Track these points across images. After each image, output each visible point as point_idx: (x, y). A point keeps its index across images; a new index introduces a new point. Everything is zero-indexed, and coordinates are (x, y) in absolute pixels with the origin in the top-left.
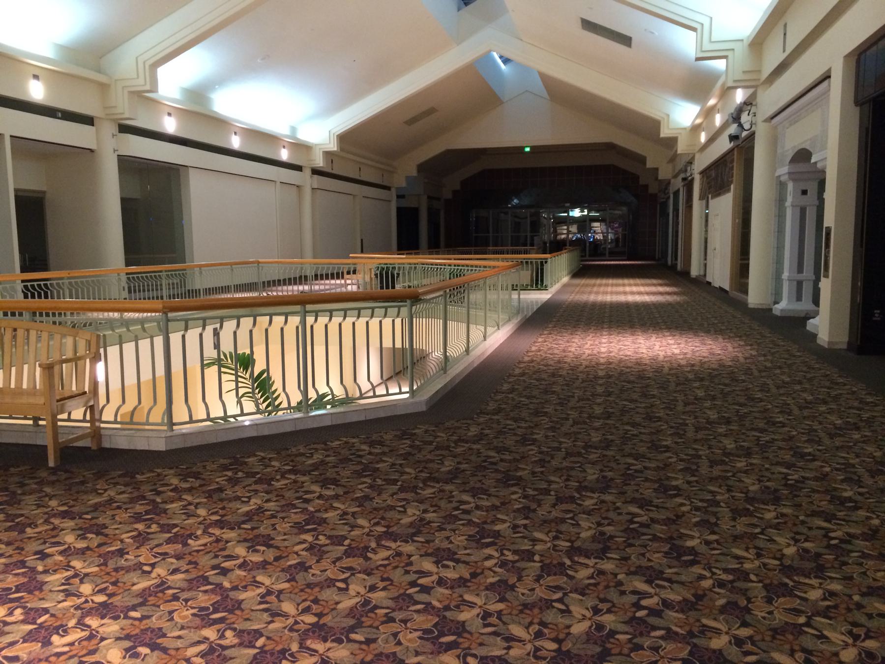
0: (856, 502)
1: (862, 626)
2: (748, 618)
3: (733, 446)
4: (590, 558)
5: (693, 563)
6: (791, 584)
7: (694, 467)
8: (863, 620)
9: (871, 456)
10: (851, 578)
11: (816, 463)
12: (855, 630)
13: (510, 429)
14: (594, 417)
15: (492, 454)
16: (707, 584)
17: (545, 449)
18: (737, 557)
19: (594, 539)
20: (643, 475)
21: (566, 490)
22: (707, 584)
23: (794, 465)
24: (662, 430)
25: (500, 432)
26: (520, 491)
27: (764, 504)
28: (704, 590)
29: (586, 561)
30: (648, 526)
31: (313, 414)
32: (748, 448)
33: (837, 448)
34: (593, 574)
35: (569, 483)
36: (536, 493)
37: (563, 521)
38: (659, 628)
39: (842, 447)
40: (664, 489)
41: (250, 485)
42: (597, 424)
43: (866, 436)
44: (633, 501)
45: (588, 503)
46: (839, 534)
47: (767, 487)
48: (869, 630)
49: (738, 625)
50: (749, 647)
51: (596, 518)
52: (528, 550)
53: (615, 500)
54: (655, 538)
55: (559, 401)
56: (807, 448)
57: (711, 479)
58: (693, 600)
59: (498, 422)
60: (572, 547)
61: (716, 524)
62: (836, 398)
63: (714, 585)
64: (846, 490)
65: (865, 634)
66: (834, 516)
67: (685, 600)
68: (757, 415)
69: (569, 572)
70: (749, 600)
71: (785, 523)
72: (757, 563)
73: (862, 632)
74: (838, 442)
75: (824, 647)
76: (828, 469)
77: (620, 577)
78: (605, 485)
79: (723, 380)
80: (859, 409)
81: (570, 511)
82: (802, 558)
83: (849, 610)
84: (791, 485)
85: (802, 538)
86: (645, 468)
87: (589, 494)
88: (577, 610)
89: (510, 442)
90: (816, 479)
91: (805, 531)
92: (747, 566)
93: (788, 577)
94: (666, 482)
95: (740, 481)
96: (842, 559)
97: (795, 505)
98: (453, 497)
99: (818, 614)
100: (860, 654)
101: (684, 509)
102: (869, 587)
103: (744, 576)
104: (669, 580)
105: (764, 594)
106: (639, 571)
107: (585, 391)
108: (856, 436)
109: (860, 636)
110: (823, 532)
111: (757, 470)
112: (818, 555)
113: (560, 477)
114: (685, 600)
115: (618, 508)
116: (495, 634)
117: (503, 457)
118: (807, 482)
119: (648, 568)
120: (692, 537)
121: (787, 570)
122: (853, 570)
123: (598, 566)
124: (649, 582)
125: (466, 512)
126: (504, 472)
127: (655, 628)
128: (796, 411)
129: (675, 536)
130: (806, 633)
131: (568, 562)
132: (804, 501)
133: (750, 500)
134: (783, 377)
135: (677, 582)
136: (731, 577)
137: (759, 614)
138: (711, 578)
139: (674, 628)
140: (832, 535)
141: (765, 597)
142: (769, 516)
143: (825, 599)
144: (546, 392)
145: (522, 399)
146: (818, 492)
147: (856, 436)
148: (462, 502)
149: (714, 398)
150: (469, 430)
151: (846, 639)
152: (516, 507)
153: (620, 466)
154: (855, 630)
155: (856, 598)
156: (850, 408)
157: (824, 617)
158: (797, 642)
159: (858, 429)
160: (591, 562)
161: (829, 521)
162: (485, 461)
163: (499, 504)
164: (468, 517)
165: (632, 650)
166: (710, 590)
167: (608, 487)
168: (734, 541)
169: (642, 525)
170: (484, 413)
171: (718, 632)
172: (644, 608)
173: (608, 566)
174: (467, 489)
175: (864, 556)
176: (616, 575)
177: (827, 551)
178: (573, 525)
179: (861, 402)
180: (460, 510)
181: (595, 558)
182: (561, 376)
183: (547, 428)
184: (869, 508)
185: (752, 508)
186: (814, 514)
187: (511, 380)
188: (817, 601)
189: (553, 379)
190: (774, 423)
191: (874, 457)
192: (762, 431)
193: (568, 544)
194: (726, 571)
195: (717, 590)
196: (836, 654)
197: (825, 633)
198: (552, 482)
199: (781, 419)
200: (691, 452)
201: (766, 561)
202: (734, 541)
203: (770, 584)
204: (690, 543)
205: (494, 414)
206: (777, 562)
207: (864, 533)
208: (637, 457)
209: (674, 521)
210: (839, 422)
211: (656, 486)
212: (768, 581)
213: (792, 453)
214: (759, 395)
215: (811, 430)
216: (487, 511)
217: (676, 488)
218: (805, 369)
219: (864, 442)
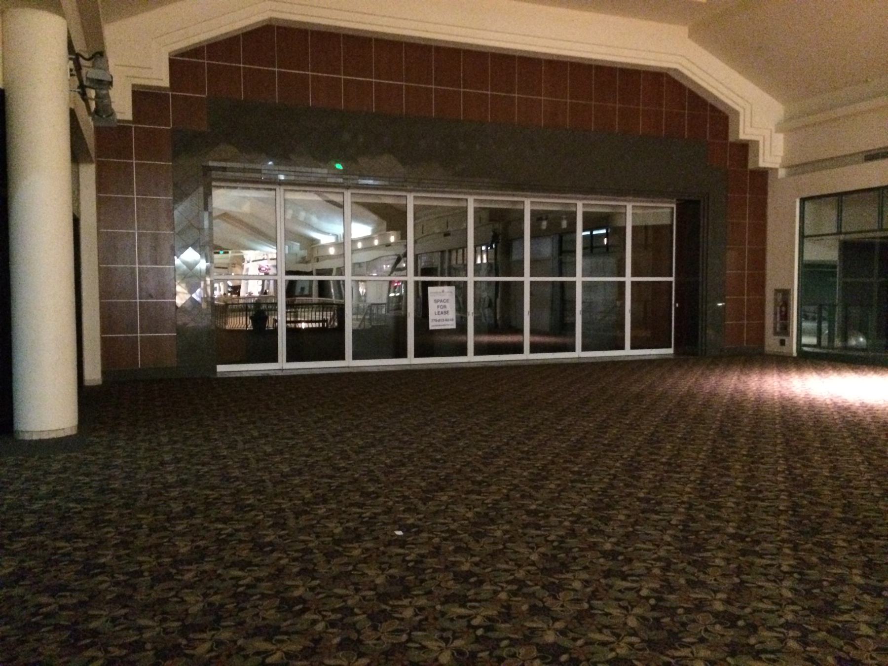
1: (449, 629)
2: (363, 649)
3: (288, 469)
4: (205, 632)
5: (303, 611)
6: (388, 608)
7: (282, 521)
8: (447, 624)
10: (377, 538)
11: (379, 499)
12: (444, 635)
13: (64, 555)
14: (174, 518)
15: (44, 599)
16: (320, 627)
18: (303, 541)
19: (204, 612)
20: (258, 591)
21: (167, 637)
22: (320, 627)
24: (284, 567)
25: (63, 518)
26: (100, 654)
28: (320, 633)
29: (190, 567)
30: (253, 586)
33: (362, 461)
34: (212, 646)
35: (162, 560)
36: (124, 652)
37: (166, 601)
38: (256, 595)
40: (259, 547)
42: (175, 493)
44: (234, 565)
45: (188, 576)
47: (318, 494)
48: (454, 632)
49: (355, 658)
50: (318, 590)
52: (136, 641)
53: (215, 568)
54: (264, 596)
55: (124, 475)
57: (300, 530)
58: (312, 645)
59: (23, 601)
60: (184, 625)
62: (381, 441)
63: (326, 627)
64: (408, 519)
65: (453, 635)
66: (364, 504)
67: (270, 574)
69: (187, 652)
70: (358, 632)
71: (371, 556)
72: (357, 598)
73: (449, 634)
74: (361, 457)
75: (425, 656)
76: (391, 503)
77: (240, 642)
78: (200, 554)
80: (373, 432)
81: (171, 589)
82: (391, 584)
83: (436, 619)
84: (366, 522)
86: (237, 530)
87: (186, 567)
88: (190, 599)
89: (67, 575)
90: (350, 483)
91: (386, 559)
92: (311, 545)
95: (298, 493)
96: (420, 577)
98: (26, 601)
99: (415, 629)
100: (453, 654)
101: (282, 562)
102: (445, 596)
103: (350, 611)
104: (286, 633)
105: (325, 558)
106: (257, 632)
107: (152, 461)
109: (449, 638)
110: (402, 557)
112: (403, 578)
113: (152, 618)
114: (270, 574)
115: (220, 575)
116: (128, 629)
117: (63, 601)
118: (425, 560)
120: (297, 587)
121: (383, 597)
122: (430, 585)
123: (216, 637)
124: (269, 639)
125: (47, 616)
126: (67, 628)
127: (252, 596)
128: (383, 478)
129: (281, 589)
130: (410, 648)
133: (338, 542)
135: (293, 633)
136: (339, 616)
137: (370, 642)
138: (323, 620)
139: (266, 592)
140: (364, 515)
141: (371, 626)
142: (356, 552)
143: (416, 615)
144: (102, 491)
145: (71, 505)
148: (40, 606)
149: (281, 453)
150: (22, 520)
151: (440, 644)
152: (108, 597)
153: (225, 584)
154: (444, 635)
155: (438, 607)
157: (420, 631)
158: (405, 658)
161: (362, 508)
164: (53, 621)
165: (239, 611)
166: (325, 632)
167: (219, 619)
169: (248, 586)
170: (50, 473)
171: (297, 587)
172: (242, 586)
173: (225, 635)
175: (435, 570)
176: (235, 642)
177: (409, 573)
178: (177, 602)
179: (400, 442)
180: (39, 615)
181: (210, 630)
182: (114, 491)
183: (116, 545)
186: (352, 505)
187: (35, 507)
188: (411, 618)
189: (108, 472)
190: (339, 469)
191: (421, 487)
193: (180, 623)
194: (334, 611)
195: (330, 630)
196: (436, 660)
197: (424, 643)
198: (144, 562)
199: (343, 465)
200: (275, 507)
201: (364, 593)
204: (297, 593)
205: (34, 534)
206: (331, 539)
207: (430, 552)
208: (226, 520)
209: (277, 576)
211: (251, 545)
212: (370, 612)
214: (320, 445)
215: (343, 451)
216: (86, 551)
217: (270, 544)
219: (411, 475)
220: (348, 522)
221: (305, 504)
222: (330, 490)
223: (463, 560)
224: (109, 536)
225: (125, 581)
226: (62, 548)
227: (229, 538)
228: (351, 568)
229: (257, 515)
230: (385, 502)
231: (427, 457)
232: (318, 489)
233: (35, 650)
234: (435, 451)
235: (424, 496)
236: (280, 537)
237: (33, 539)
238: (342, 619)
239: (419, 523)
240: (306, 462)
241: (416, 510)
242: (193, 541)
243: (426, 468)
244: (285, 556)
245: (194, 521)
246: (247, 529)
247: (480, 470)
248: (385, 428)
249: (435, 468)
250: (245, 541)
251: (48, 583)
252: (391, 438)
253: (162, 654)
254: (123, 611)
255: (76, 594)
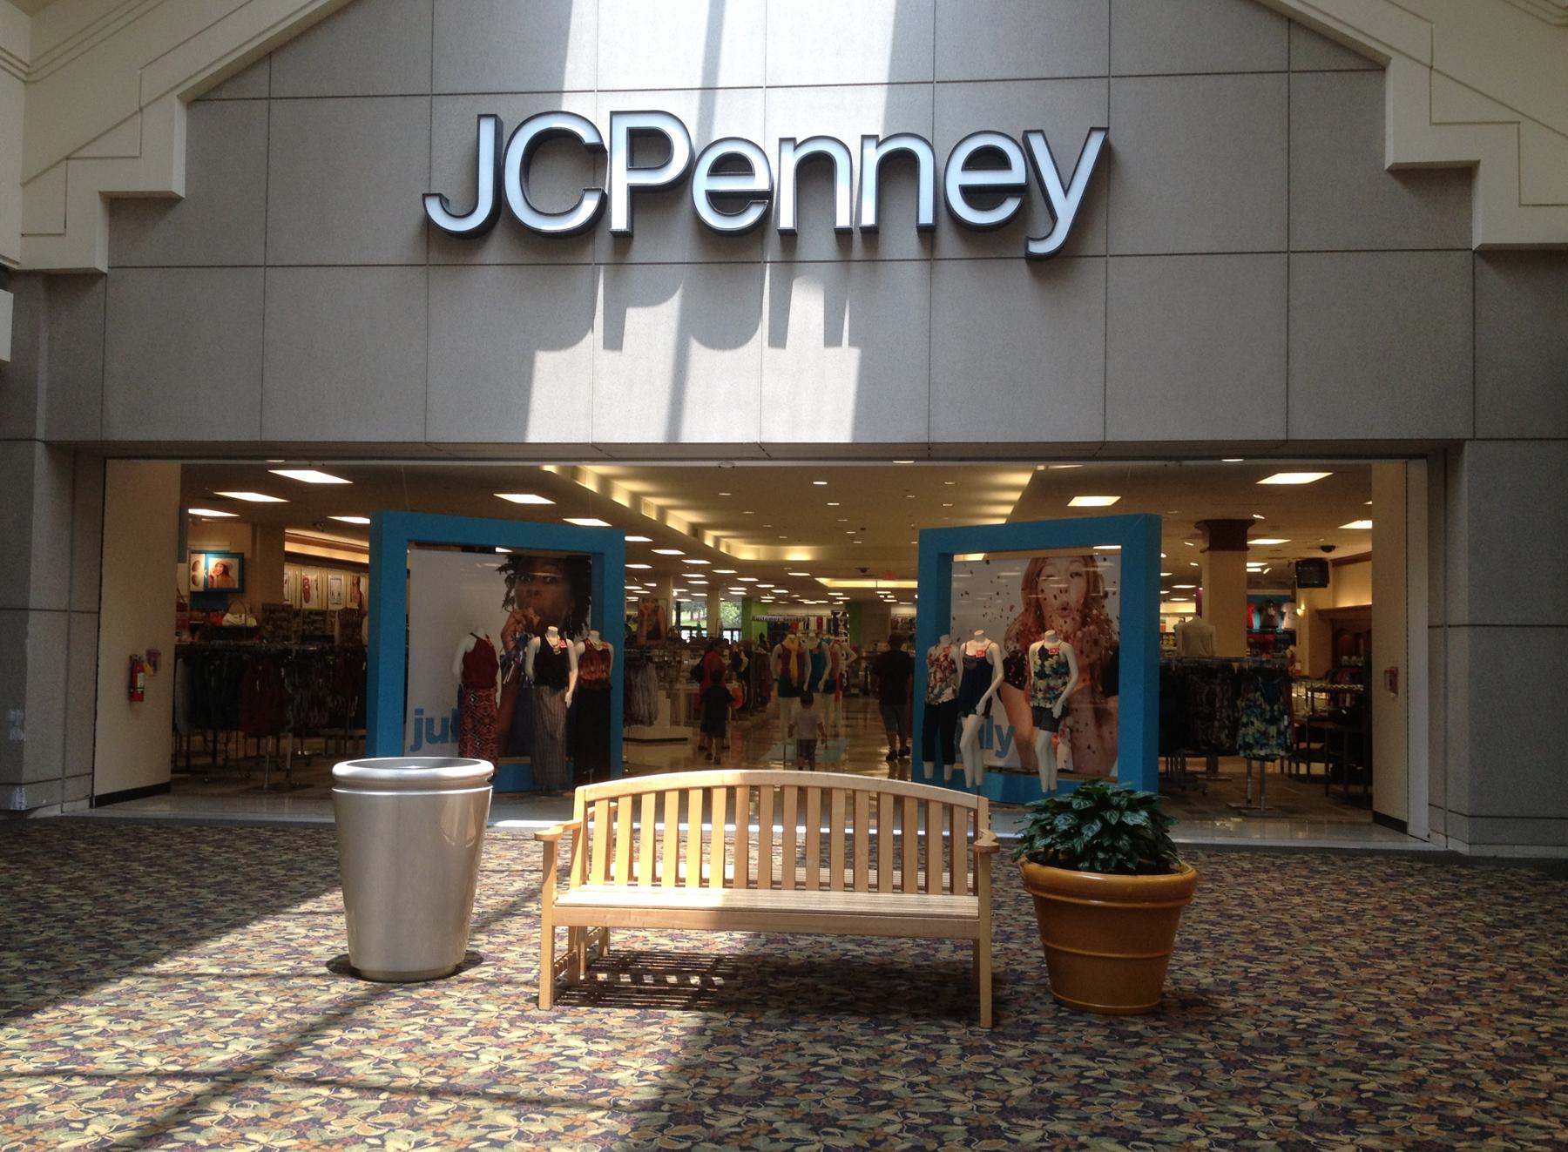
0: (1479, 1124)
6: (1312, 1140)
9: (1486, 1047)
10: (1391, 1133)
11: (1400, 1060)
17: (919, 1121)
23: (1365, 1066)
24: (1154, 1066)
26: (897, 1119)
27: (1332, 1133)
31: (1108, 501)
32: (1234, 983)
39: (1370, 981)
41: (375, 1113)
43: (1472, 1014)
46: (1372, 1086)
51: (1029, 1073)
53: (1076, 1132)
55: (914, 1054)
56: (1379, 1035)
59: (797, 1049)
60: (1004, 1107)
61: (1203, 1079)
64: (1460, 1106)
66: (1304, 1006)
68: (1240, 938)
71: (1298, 1075)
76: (1423, 1071)
79: (1205, 915)
81: (988, 1064)
82: (1264, 1040)
85: (1324, 1092)
87: (1023, 1122)
93: (1308, 1134)
94: (1157, 1100)
97: (1383, 1133)
108: (1457, 1014)
110: (1350, 1084)
111: (1305, 1076)
115: (1057, 1060)
119: (1119, 1129)
120: (894, 1079)
126: (856, 1085)
128: (1346, 972)
131: (1004, 1125)
132: (1268, 993)
134: (1309, 911)
146: (1341, 1037)
147: (1457, 1014)
153: (1064, 1072)
156: (1434, 965)
159: (1392, 956)
160: (1037, 1123)
162: (815, 1064)
163: (876, 1057)
168: (1231, 1097)
174: (797, 1116)
184: (1505, 1135)
185: (1312, 1140)
190: (1267, 949)
191: (1493, 1050)
192: (1250, 960)
202: (1231, 1097)
203: (1286, 1142)
210: (1422, 990)
212: (1282, 1139)
213: (1356, 1044)
218: (1343, 896)
219: (1471, 1023)
220: (1328, 1094)
221: (1242, 1049)
222: (1246, 978)
223: (1460, 1101)
224: (895, 1047)
225: (926, 1126)
226: (828, 1057)
227: (1100, 1086)
228: (1262, 1084)
229: (1148, 1055)
230: (1412, 1067)
231: (1443, 949)
232: (1225, 973)
233: (818, 1102)
234: (1464, 941)
235: (1500, 1066)
236: (1194, 1099)
237: (782, 1035)
238: (1235, 1141)
239: (1485, 1118)
240: (1246, 970)
241: (1478, 1092)
242: (1035, 1080)
243: (1507, 1012)
244: (1201, 1133)
245: (1035, 1046)
246: (1132, 1076)
247: (1545, 980)
248: (1369, 896)
249: (1531, 1015)
250: (1127, 1097)
251: (807, 1109)
252: (1428, 944)
253: (975, 1132)
254: (925, 1078)
255: (851, 1134)
